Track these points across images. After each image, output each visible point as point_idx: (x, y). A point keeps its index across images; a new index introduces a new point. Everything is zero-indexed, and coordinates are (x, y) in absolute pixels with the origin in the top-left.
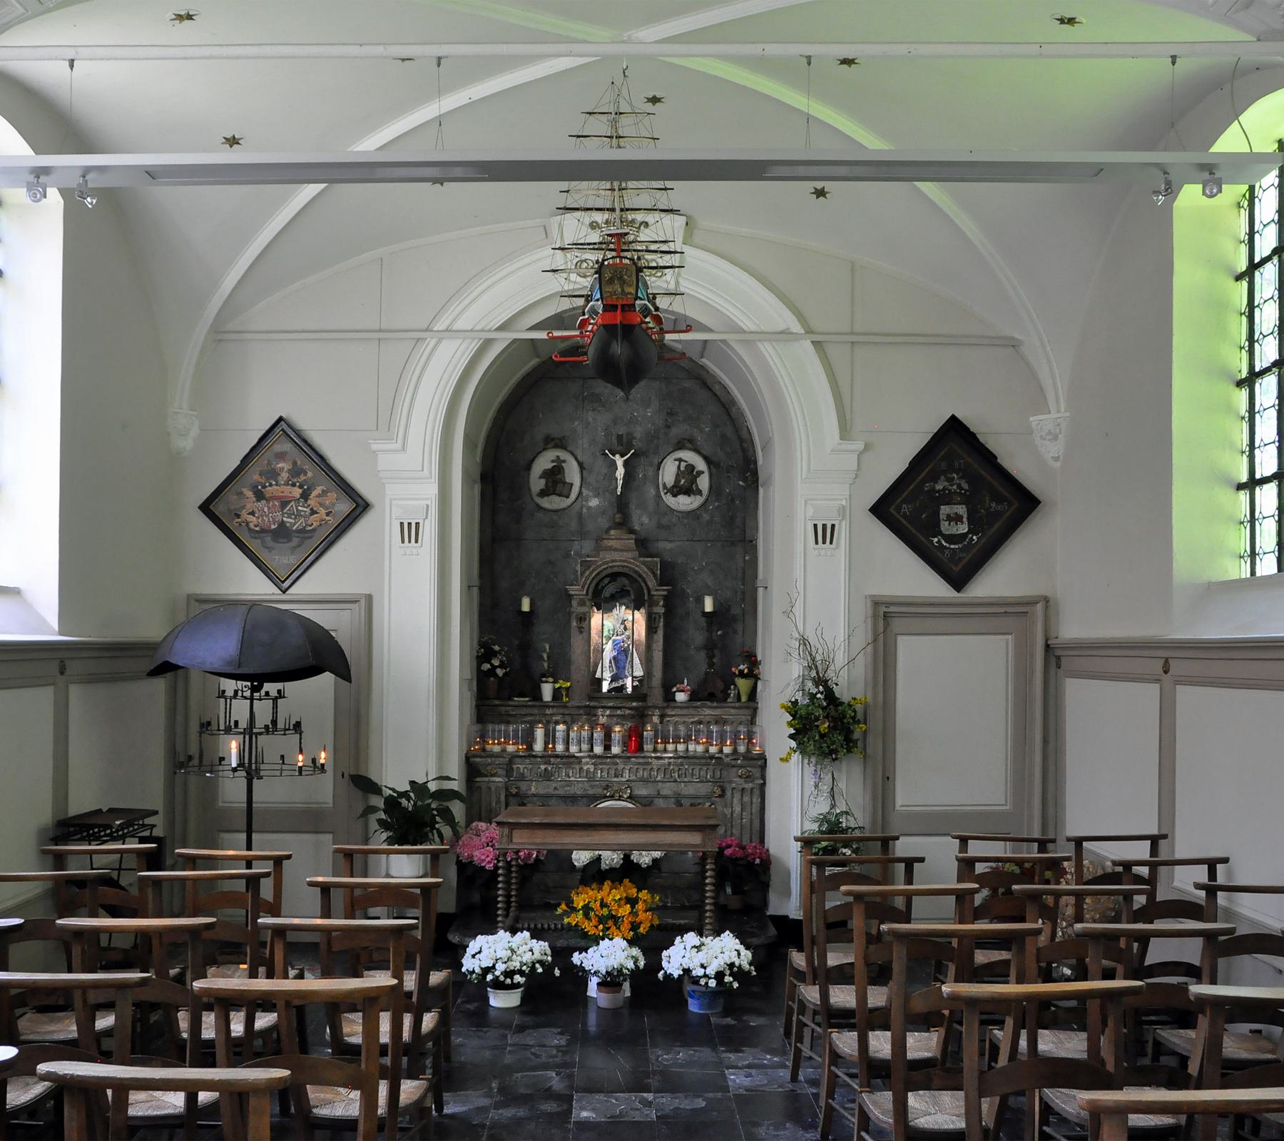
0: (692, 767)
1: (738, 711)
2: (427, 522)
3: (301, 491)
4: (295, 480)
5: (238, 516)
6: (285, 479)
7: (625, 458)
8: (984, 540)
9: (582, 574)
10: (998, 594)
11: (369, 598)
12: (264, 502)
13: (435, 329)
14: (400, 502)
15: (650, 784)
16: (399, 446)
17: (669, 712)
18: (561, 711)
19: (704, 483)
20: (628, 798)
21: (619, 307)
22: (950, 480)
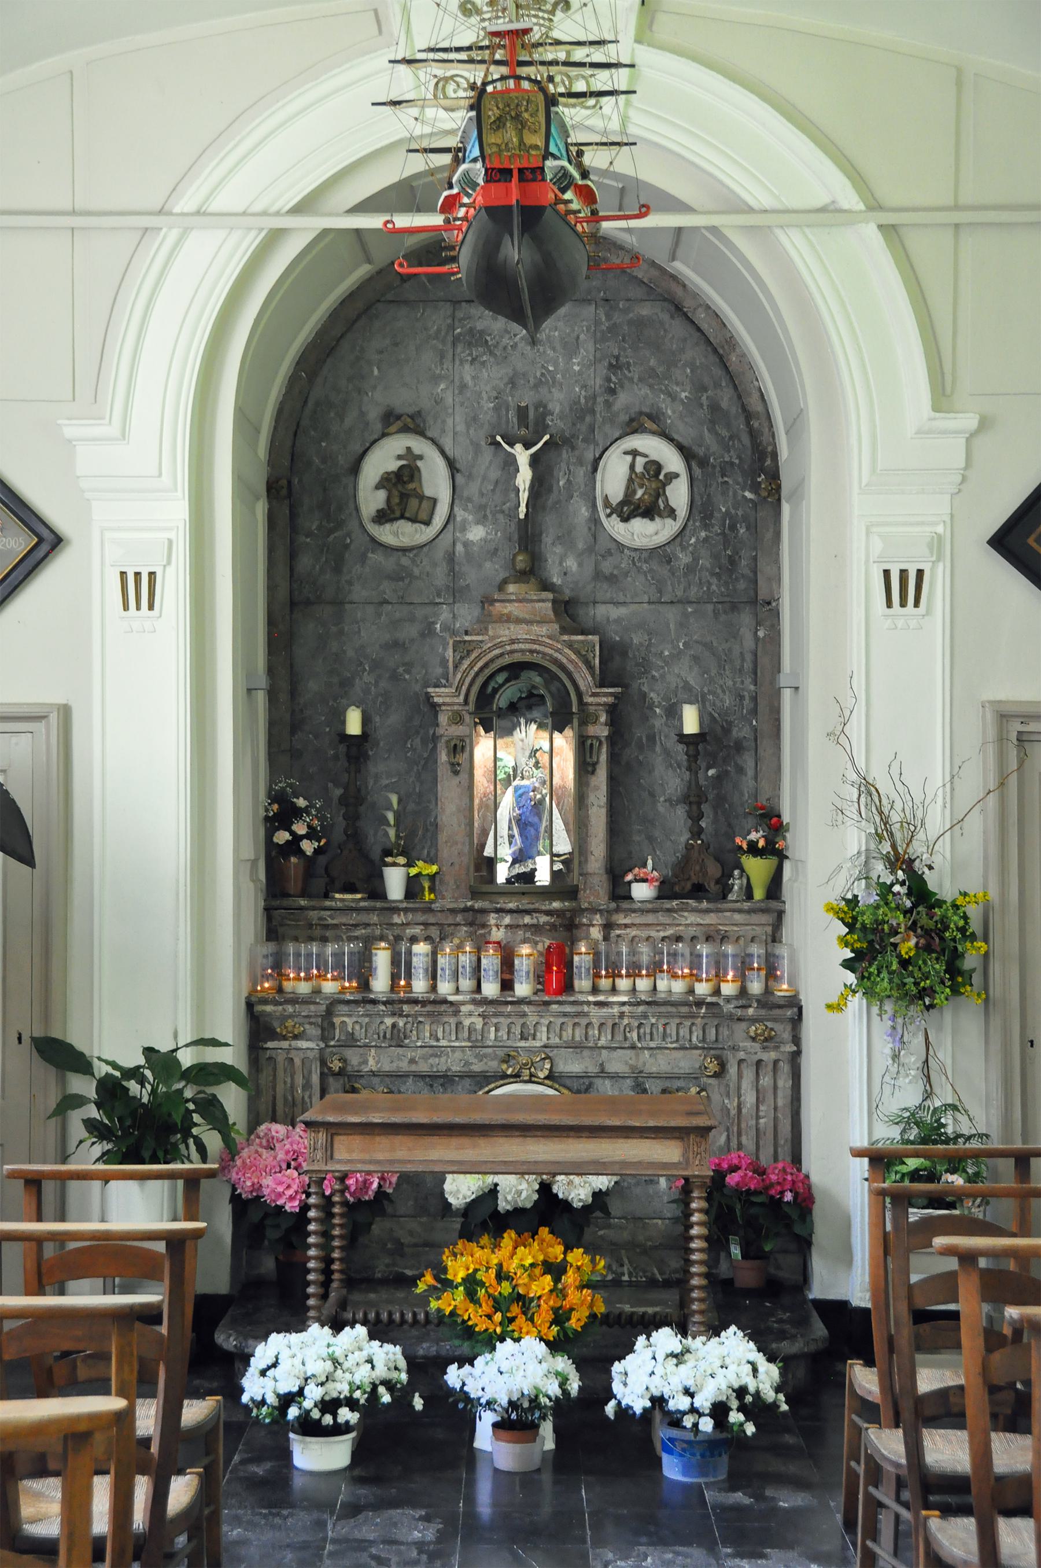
0: (663, 1021)
2: (171, 571)
11: (65, 712)
15: (586, 1053)
16: (114, 430)
17: (621, 919)
18: (421, 918)
19: (679, 495)
20: (546, 1078)
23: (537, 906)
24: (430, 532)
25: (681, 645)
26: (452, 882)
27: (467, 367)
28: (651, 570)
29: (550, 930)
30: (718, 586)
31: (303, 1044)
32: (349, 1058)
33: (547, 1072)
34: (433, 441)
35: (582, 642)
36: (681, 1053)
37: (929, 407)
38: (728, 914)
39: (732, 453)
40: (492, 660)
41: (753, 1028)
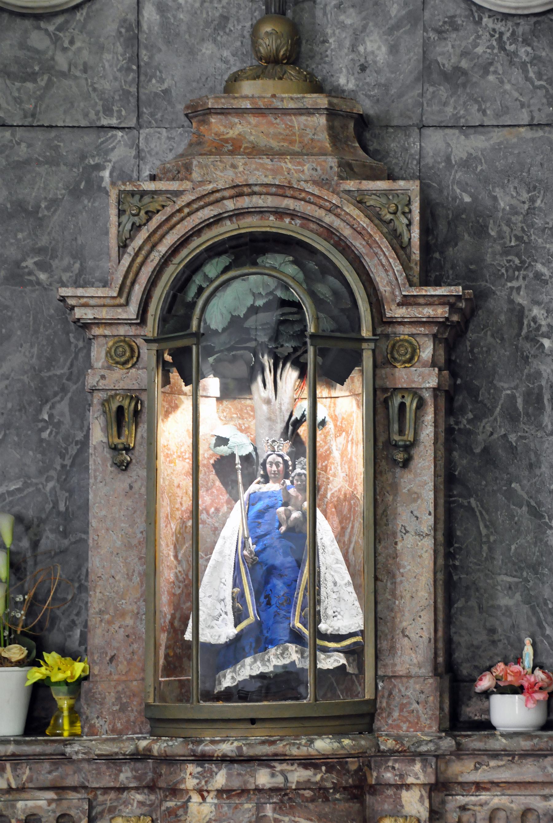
9: (123, 246)
23: (279, 747)
26: (110, 698)
28: (536, 59)
35: (385, 193)
40: (197, 232)
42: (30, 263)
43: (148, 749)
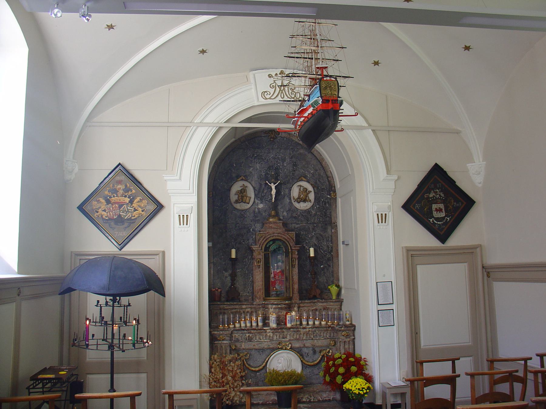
0: (320, 332)
1: (334, 303)
2: (192, 215)
3: (129, 199)
4: (126, 194)
5: (97, 212)
6: (121, 193)
7: (276, 185)
8: (452, 220)
10: (462, 244)
11: (164, 253)
12: (110, 205)
13: (195, 122)
14: (179, 205)
15: (300, 341)
16: (178, 177)
17: (302, 305)
18: (249, 306)
19: (312, 196)
20: (290, 349)
21: (330, 101)
22: (436, 193)
23: (282, 302)
24: (249, 206)
25: (313, 234)
27: (258, 164)
29: (285, 309)
30: (322, 219)
31: (225, 342)
32: (237, 345)
33: (290, 347)
34: (250, 183)
36: (325, 340)
37: (386, 174)
38: (329, 303)
39: (324, 186)
41: (343, 333)
42: (242, 241)
43: (265, 303)
